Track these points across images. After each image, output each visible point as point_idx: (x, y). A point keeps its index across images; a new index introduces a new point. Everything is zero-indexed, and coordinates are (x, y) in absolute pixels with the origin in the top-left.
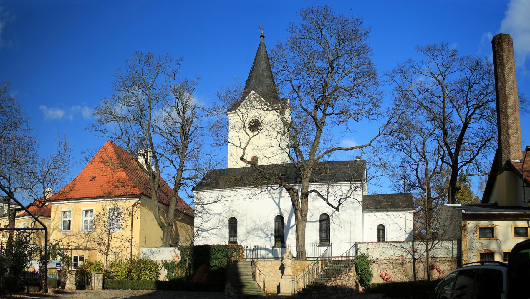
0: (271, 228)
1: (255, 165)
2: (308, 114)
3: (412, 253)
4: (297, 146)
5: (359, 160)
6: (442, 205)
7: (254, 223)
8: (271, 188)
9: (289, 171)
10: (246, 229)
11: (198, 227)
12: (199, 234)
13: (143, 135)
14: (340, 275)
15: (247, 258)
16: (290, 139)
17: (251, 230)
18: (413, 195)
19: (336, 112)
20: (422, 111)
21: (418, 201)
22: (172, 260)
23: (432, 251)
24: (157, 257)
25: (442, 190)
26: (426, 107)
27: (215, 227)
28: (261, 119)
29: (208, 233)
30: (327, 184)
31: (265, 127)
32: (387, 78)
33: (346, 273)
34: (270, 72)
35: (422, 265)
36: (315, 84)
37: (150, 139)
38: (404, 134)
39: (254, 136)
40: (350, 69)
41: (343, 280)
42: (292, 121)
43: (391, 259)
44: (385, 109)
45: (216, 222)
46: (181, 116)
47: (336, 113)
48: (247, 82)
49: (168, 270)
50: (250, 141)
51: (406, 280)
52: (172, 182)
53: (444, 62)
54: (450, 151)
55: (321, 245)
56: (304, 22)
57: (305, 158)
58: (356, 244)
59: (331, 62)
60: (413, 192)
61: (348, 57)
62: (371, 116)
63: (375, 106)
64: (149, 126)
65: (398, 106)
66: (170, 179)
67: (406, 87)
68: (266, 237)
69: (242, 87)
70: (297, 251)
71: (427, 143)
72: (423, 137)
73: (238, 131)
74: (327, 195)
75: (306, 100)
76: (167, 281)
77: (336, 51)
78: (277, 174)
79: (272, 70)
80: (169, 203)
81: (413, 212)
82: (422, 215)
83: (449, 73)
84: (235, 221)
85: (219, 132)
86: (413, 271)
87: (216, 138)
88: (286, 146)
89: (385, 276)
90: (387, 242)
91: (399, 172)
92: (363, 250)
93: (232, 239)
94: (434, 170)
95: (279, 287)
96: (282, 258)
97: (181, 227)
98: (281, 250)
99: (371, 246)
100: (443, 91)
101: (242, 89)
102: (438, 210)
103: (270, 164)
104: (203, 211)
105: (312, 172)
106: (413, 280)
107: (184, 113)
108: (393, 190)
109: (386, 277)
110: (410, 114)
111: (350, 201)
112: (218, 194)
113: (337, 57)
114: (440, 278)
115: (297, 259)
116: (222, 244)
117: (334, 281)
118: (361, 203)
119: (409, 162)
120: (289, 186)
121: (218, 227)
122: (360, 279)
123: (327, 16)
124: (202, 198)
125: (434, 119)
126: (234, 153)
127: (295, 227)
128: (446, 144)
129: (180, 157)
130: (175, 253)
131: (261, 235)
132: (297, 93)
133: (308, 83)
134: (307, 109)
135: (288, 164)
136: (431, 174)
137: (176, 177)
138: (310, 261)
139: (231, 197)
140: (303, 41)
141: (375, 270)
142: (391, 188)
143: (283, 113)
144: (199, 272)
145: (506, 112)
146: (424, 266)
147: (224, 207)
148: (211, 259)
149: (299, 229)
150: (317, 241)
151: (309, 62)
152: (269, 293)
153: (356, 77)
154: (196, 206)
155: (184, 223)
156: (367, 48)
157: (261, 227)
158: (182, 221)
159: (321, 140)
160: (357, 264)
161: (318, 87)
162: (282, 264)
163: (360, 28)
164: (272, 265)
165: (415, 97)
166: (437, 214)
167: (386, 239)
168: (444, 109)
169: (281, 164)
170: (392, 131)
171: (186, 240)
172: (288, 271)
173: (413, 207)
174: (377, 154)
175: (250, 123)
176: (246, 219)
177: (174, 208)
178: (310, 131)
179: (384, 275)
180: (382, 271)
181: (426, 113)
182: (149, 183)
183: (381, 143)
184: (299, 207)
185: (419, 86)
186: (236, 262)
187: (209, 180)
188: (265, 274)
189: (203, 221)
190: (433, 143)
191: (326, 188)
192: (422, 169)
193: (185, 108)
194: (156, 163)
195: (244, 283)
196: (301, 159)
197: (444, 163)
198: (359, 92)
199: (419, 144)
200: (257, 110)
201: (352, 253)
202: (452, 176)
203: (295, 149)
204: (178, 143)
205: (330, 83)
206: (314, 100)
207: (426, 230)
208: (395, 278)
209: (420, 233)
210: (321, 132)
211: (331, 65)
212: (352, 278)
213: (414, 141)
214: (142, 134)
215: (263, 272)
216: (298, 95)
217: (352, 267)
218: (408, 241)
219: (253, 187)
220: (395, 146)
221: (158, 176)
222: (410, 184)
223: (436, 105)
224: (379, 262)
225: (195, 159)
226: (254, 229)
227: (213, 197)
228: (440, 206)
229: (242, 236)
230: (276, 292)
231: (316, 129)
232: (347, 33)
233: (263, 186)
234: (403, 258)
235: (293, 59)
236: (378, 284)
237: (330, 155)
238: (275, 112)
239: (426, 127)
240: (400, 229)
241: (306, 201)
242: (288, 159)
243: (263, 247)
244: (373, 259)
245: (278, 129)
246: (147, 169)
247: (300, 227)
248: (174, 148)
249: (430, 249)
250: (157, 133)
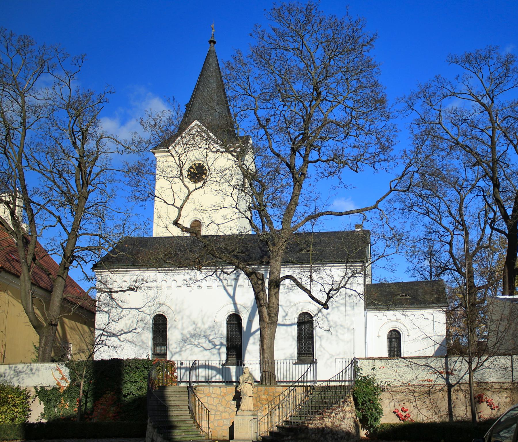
0: (221, 334)
1: (196, 235)
2: (280, 161)
3: (445, 376)
4: (263, 208)
5: (359, 230)
6: (493, 297)
7: (194, 326)
8: (222, 271)
9: (251, 246)
10: (182, 334)
11: (102, 330)
12: (103, 341)
13: (8, 169)
14: (330, 411)
15: (181, 382)
16: (252, 198)
17: (188, 336)
18: (445, 283)
19: (324, 158)
20: (458, 152)
21: (453, 292)
22: (54, 384)
23: (477, 373)
24: (25, 380)
25: (492, 274)
26: (463, 147)
27: (131, 330)
28: (208, 165)
29: (119, 339)
30: (309, 267)
31: (215, 176)
32: (402, 105)
33: (339, 407)
34: (223, 96)
35: (461, 395)
36: (293, 115)
37: (22, 178)
38: (430, 189)
39: (196, 189)
40: (345, 94)
41: (335, 419)
42: (256, 171)
43: (411, 385)
44: (400, 153)
45: (132, 322)
46: (78, 148)
47: (324, 160)
48: (187, 106)
49: (47, 403)
50: (190, 197)
51: (436, 419)
52: (59, 253)
53: (492, 76)
54: (505, 211)
55: (300, 361)
56: (277, 25)
57: (275, 227)
58: (355, 362)
59: (317, 84)
60: (445, 278)
61: (342, 77)
62: (377, 164)
63: (384, 148)
64: (20, 155)
65: (420, 147)
66: (54, 247)
67: (432, 119)
68: (212, 348)
69: (179, 113)
70: (262, 371)
71: (466, 201)
72: (459, 193)
73: (171, 179)
74: (309, 283)
75: (278, 139)
76: (43, 423)
77: (324, 67)
78: (231, 250)
79: (227, 93)
80: (52, 287)
81: (445, 310)
82: (460, 314)
83: (501, 91)
84: (163, 321)
85: (140, 179)
86: (447, 405)
87: (135, 188)
88: (246, 207)
89: (401, 412)
90: (404, 358)
91: (423, 248)
92: (365, 370)
93: (158, 350)
94: (479, 243)
95: (232, 429)
96: (238, 382)
97: (71, 328)
98: (237, 369)
99: (378, 364)
100: (491, 120)
101: (179, 116)
102: (486, 306)
103: (222, 234)
104: (111, 303)
105: (287, 248)
106: (447, 420)
107: (83, 144)
108: (413, 275)
109: (404, 414)
110: (438, 158)
111: (346, 294)
112: (136, 277)
113: (326, 77)
114: (492, 417)
115: (262, 384)
116: (141, 358)
117: (320, 420)
118: (363, 296)
119: (437, 232)
120: (250, 268)
121: (135, 329)
122: (361, 418)
123: (311, 17)
124: (110, 281)
125: (478, 163)
126: (163, 214)
127: (259, 332)
128: (498, 201)
129: (74, 213)
130: (61, 372)
131: (204, 345)
132: (264, 128)
133: (282, 115)
134: (280, 154)
135: (249, 235)
136: (474, 249)
137: (65, 244)
138: (282, 386)
139: (158, 283)
140: (275, 52)
141: (385, 402)
142: (410, 273)
143: (243, 158)
144: (101, 404)
146: (465, 396)
147: (146, 297)
148: (124, 383)
149: (265, 336)
150: (293, 355)
151: (283, 84)
152: (216, 438)
153: (355, 105)
154: (98, 295)
155: (78, 322)
156: (372, 62)
157: (205, 332)
158: (75, 318)
159: (300, 200)
160: (356, 393)
161: (297, 120)
162: (237, 392)
163: (361, 34)
164: (222, 394)
165: (447, 132)
166: (485, 313)
167: (402, 353)
168: (493, 147)
169: (237, 235)
170: (410, 185)
171: (80, 351)
172: (247, 403)
173: (446, 302)
174: (387, 221)
175: (190, 169)
176: (182, 318)
177: (60, 296)
178: (283, 186)
179: (400, 411)
180: (397, 404)
181: (464, 155)
182: (16, 251)
183: (393, 204)
184: (265, 302)
185: (453, 115)
186: (163, 388)
187: (122, 253)
188: (210, 407)
189: (111, 320)
190: (476, 201)
191: (307, 273)
192: (459, 242)
193: (86, 136)
194: (30, 218)
195: (176, 423)
196: (270, 227)
197: (494, 232)
198: (360, 128)
199: (454, 203)
200: (202, 150)
201: (348, 375)
202: (508, 251)
203: (260, 213)
204: (71, 190)
205: (314, 114)
206: (290, 140)
207: (468, 338)
208: (417, 415)
209: (457, 343)
210: (301, 188)
211: (316, 89)
212: (349, 415)
213: (445, 199)
214: (6, 167)
215: (206, 405)
216: (266, 132)
217: (349, 397)
218: (438, 357)
219: (194, 268)
220: (416, 208)
221: (33, 242)
222: (440, 267)
223: (480, 143)
224: (393, 389)
225: (99, 219)
226: (193, 336)
227: (128, 281)
228: (490, 300)
229: (174, 345)
230: (227, 438)
231: (292, 184)
232: (341, 41)
233: (209, 268)
234: (430, 383)
235: (258, 78)
236: (391, 425)
237: (314, 223)
238: (230, 156)
239: (464, 177)
240: (424, 336)
241: (276, 292)
242: (249, 227)
243: (207, 364)
244: (382, 384)
245: (234, 182)
246: (13, 228)
247: (267, 333)
248: (63, 198)
249: (474, 370)
250: (35, 170)
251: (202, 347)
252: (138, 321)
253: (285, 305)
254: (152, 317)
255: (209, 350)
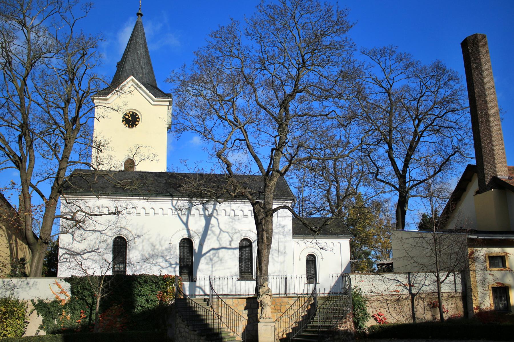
3: (408, 287)
22: (52, 298)
27: (93, 249)
45: (95, 243)
49: (45, 315)
51: (403, 321)
86: (411, 310)
98: (190, 284)
106: (411, 321)
130: (59, 287)
145: (488, 121)
146: (424, 303)
164: (234, 304)
176: (143, 241)
180: (374, 310)
234: (398, 293)
251: (159, 265)
252: (100, 242)
253: (231, 232)
254: (113, 239)
255: (166, 268)
